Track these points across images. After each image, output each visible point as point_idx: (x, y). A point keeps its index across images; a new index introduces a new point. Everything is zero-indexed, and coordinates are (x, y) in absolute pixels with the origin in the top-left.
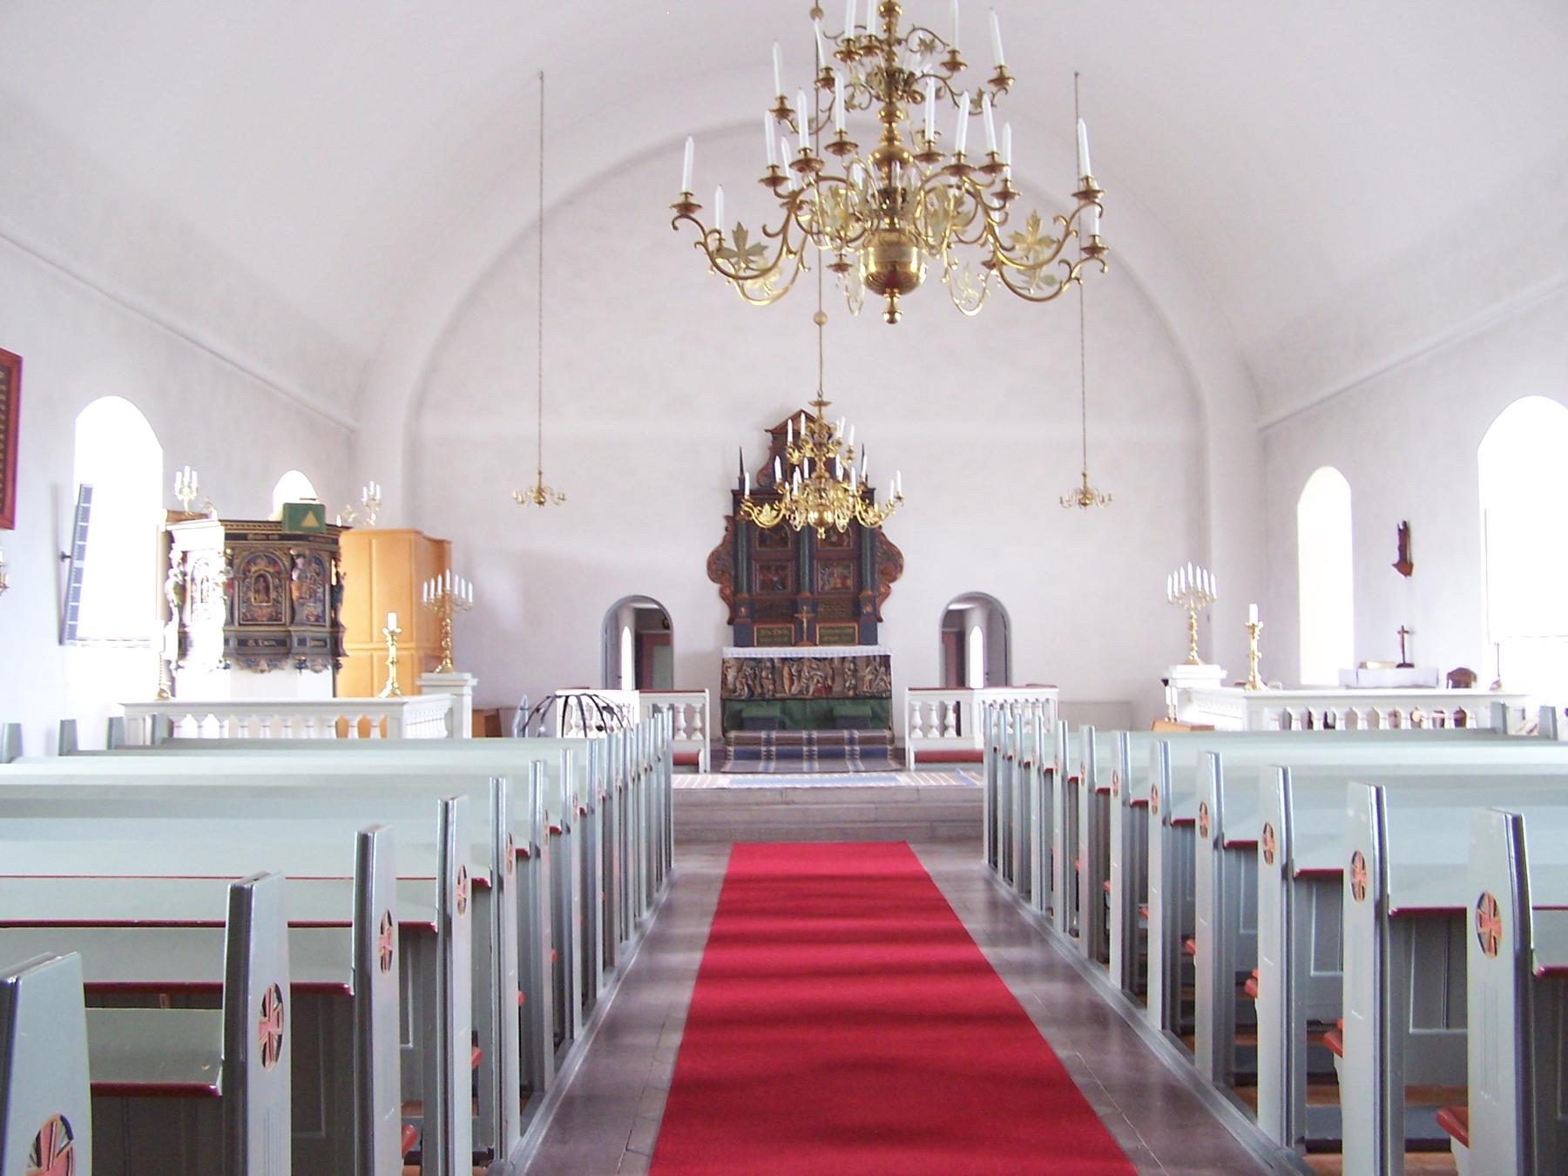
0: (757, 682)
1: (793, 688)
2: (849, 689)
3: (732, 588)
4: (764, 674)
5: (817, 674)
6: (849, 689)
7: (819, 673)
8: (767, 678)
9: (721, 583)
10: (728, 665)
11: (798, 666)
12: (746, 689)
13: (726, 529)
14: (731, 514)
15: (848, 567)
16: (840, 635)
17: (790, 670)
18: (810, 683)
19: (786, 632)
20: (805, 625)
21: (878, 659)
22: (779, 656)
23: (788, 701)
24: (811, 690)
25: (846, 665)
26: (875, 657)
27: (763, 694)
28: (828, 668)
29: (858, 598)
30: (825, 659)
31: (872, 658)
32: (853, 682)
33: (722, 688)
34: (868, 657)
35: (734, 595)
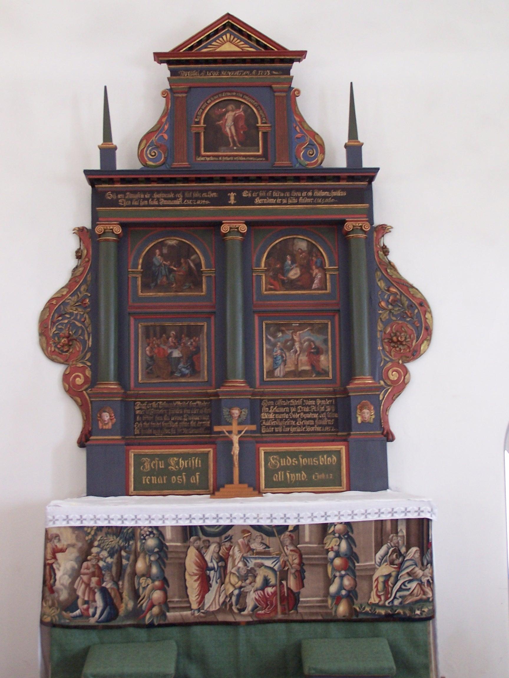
0: (125, 585)
1: (209, 597)
2: (338, 598)
3: (88, 373)
4: (140, 565)
5: (261, 565)
6: (338, 598)
7: (268, 563)
8: (147, 574)
9: (65, 362)
10: (59, 546)
11: (220, 545)
12: (99, 602)
13: (79, 255)
14: (88, 225)
15: (322, 330)
16: (309, 469)
17: (202, 557)
18: (248, 588)
19: (196, 462)
20: (236, 449)
21: (402, 529)
22: (174, 523)
23: (197, 629)
24: (250, 602)
25: (331, 543)
26: (395, 522)
27: (137, 612)
28: (289, 549)
29: (345, 391)
30: (282, 529)
31: (389, 526)
32: (347, 582)
33: (44, 598)
34: (381, 523)
35: (92, 386)
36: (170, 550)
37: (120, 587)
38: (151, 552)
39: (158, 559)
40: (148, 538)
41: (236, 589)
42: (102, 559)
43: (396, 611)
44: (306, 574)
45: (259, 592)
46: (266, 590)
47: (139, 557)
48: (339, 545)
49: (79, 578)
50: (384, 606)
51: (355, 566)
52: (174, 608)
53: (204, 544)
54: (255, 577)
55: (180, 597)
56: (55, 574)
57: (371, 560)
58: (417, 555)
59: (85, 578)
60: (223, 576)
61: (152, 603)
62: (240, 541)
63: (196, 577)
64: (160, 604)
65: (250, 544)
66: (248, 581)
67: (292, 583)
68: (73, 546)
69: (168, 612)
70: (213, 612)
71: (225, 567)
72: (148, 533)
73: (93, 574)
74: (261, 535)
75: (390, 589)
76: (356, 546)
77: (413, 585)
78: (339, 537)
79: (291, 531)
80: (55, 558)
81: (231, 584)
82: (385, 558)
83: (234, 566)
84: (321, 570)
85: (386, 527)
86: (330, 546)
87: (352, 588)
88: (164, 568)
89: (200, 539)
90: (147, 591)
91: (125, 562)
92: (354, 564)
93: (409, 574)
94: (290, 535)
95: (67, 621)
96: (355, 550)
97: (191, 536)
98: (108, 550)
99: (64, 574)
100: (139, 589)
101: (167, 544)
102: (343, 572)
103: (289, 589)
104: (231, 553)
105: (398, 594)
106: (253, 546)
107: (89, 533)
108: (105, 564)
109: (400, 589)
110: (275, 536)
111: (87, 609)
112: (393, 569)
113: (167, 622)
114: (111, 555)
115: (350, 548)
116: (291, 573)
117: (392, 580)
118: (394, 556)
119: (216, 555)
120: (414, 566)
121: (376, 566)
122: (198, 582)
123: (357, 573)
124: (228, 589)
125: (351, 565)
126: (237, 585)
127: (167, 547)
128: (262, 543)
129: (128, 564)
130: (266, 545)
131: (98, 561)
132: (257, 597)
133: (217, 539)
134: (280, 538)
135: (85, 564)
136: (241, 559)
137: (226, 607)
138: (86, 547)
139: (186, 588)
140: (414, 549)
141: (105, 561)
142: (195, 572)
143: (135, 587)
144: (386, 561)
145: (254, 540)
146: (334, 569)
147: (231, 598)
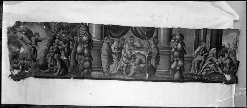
0: (71, 57)
1: (112, 66)
4: (79, 49)
6: (175, 71)
7: (142, 52)
11: (119, 42)
17: (110, 47)
36: (94, 43)
37: (69, 59)
38: (85, 43)
39: (88, 46)
40: (83, 36)
41: (125, 64)
42: (60, 45)
43: (202, 78)
44: (160, 59)
45: (137, 66)
46: (140, 65)
47: (79, 44)
48: (177, 46)
49: (49, 54)
50: (197, 75)
51: (184, 56)
52: (94, 70)
53: (111, 41)
54: (135, 59)
55: (98, 65)
56: (37, 52)
57: (192, 54)
58: (215, 52)
59: (51, 54)
60: (119, 58)
61: (84, 67)
62: (129, 41)
63: (106, 57)
64: (88, 69)
65: (133, 43)
66: (131, 61)
67: (153, 62)
68: (46, 39)
69: (92, 72)
70: (114, 74)
71: (121, 53)
72: (83, 33)
73: (56, 52)
74: (139, 39)
75: (200, 67)
76: (185, 46)
77: (212, 65)
78: (178, 42)
79: (154, 38)
80: (36, 44)
81: (123, 61)
82: (199, 53)
83: (125, 53)
84: (168, 57)
85: (200, 39)
86: (173, 46)
87: (182, 66)
88: (90, 51)
89: (109, 39)
90: (82, 62)
91: (71, 47)
92: (184, 55)
93: (210, 60)
94: (153, 40)
95: (43, 74)
96: (185, 49)
97: (105, 37)
98: (63, 41)
99: (41, 52)
100: (78, 60)
101: (93, 40)
102: (178, 59)
103: (151, 65)
104: (124, 46)
105: (205, 70)
106: (135, 44)
107: (54, 32)
108: (61, 47)
109: (206, 67)
110: (146, 40)
111: (53, 69)
112: (203, 58)
113: (91, 77)
114: (65, 43)
115: (183, 48)
116: (153, 58)
117: (202, 63)
118: (204, 52)
119: (116, 47)
120: (213, 57)
121: (195, 56)
122: (107, 59)
123: (185, 59)
124: (122, 64)
125: (182, 55)
126: (126, 62)
127: (93, 41)
128: (139, 43)
129: (73, 48)
130: (141, 44)
131: (58, 46)
132: (136, 68)
133: (118, 39)
134: (148, 41)
135: (51, 47)
136: (129, 50)
137: (120, 71)
138: (52, 39)
139: (101, 61)
140: (213, 49)
141: (62, 46)
142: (106, 54)
143: (76, 59)
144: (199, 54)
145: (136, 41)
146: (174, 57)
147: (123, 68)
